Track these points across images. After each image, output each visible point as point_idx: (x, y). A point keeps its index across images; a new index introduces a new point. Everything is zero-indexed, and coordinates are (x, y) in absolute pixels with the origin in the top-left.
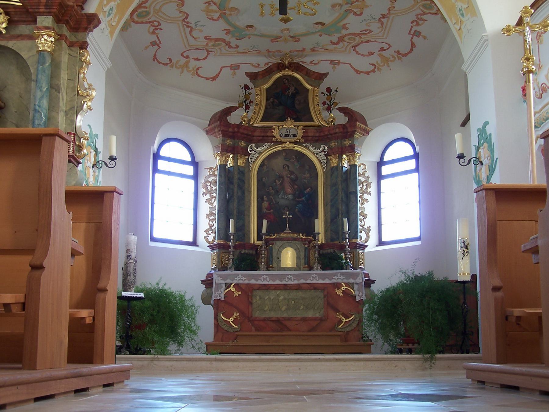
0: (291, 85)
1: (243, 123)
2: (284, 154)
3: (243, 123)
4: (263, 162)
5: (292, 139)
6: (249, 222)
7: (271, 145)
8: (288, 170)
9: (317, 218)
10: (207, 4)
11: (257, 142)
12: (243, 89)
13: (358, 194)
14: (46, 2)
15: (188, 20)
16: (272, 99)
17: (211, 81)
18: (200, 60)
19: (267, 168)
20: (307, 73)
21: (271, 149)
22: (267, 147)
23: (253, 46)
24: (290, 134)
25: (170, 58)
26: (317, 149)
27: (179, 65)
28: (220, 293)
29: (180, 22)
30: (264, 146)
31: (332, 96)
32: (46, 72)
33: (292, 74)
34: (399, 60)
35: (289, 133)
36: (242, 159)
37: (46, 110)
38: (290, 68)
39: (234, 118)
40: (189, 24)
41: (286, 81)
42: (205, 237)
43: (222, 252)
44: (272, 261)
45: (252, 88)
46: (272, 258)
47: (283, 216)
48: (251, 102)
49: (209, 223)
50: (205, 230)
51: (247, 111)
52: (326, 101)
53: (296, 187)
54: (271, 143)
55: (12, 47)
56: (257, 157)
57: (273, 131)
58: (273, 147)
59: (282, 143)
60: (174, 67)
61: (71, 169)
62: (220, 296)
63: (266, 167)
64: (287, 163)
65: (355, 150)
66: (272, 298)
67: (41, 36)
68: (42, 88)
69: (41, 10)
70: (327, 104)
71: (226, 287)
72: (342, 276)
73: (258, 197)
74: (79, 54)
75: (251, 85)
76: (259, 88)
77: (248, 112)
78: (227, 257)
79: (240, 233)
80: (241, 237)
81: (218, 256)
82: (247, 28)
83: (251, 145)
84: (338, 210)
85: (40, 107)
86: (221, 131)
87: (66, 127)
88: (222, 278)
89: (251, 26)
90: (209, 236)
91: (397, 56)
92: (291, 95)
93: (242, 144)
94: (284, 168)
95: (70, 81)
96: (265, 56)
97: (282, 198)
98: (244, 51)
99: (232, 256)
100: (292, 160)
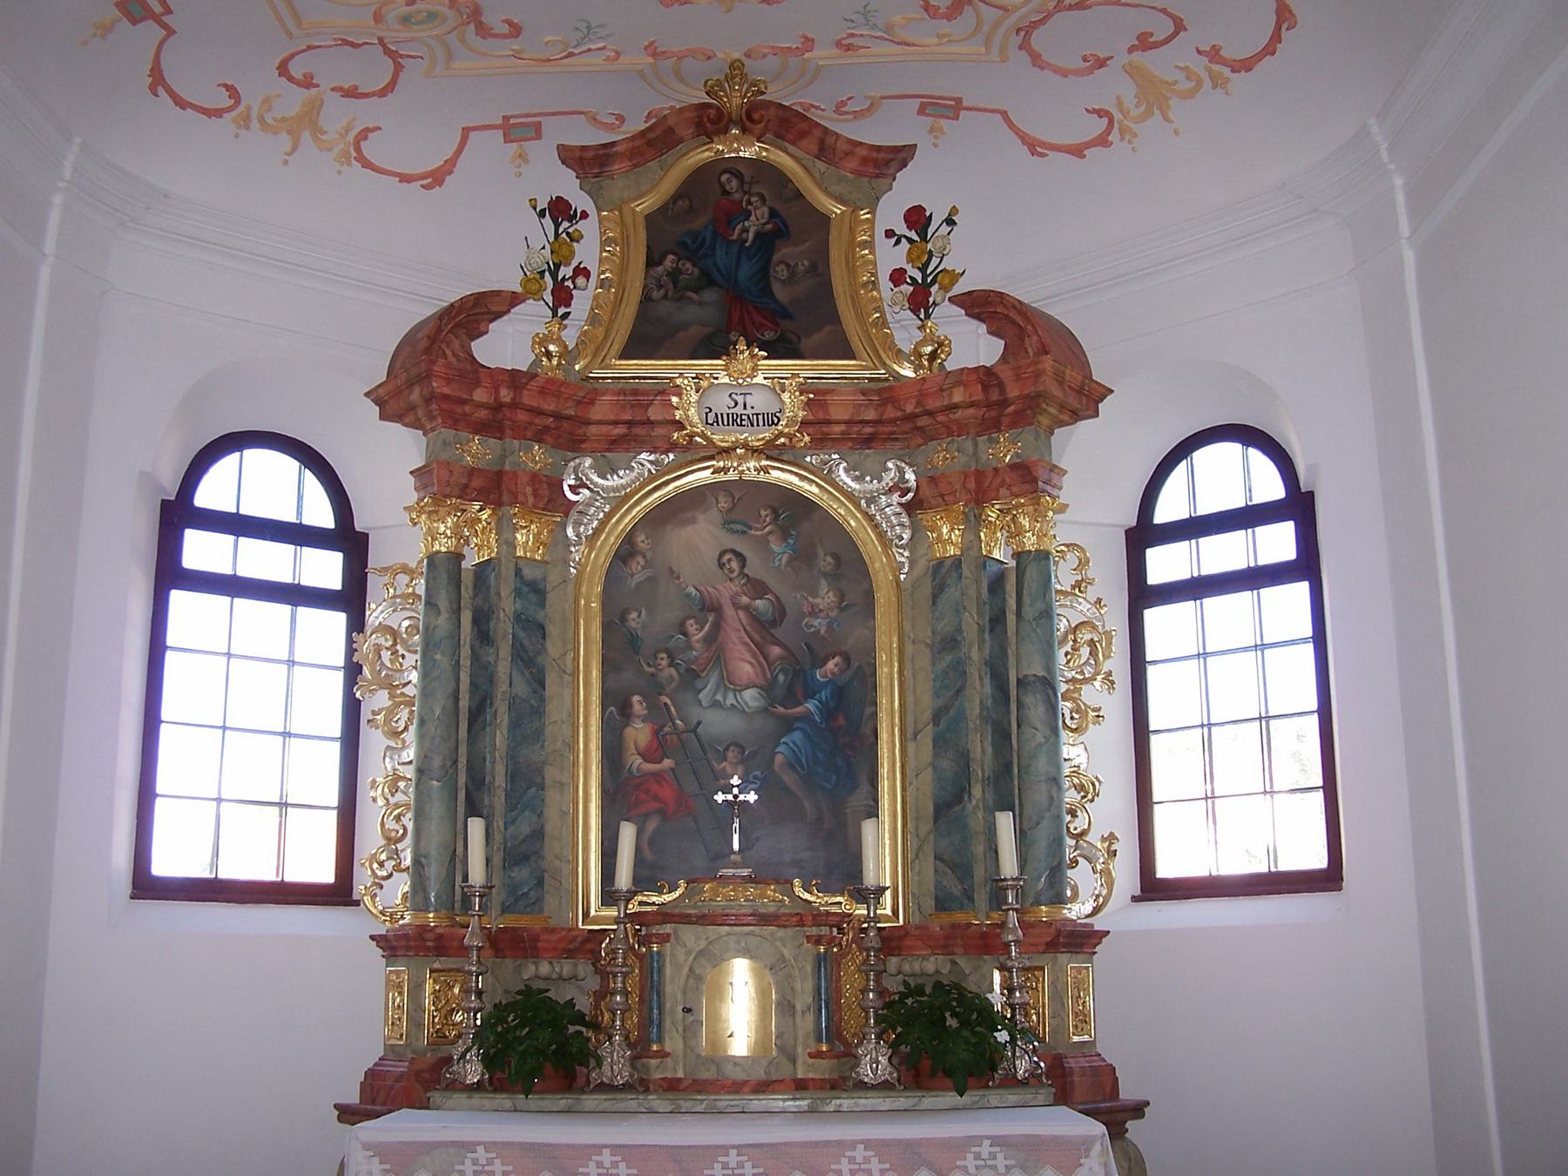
0: (753, 199)
2: (724, 503)
4: (629, 538)
8: (742, 574)
9: (873, 812)
11: (608, 450)
12: (544, 216)
16: (671, 257)
17: (422, 186)
19: (644, 568)
20: (827, 148)
23: (583, 26)
24: (749, 411)
26: (868, 478)
31: (929, 246)
34: (1214, 87)
35: (745, 408)
38: (748, 124)
41: (734, 183)
43: (431, 972)
45: (584, 215)
46: (660, 1009)
47: (716, 797)
48: (581, 271)
51: (561, 311)
52: (905, 266)
53: (776, 651)
60: (255, 124)
65: (1040, 483)
70: (911, 277)
72: (1000, 1156)
75: (580, 200)
77: (566, 315)
78: (876, 316)
79: (522, 873)
80: (525, 890)
84: (964, 759)
88: (388, 1167)
91: (1209, 71)
92: (754, 241)
93: (537, 456)
94: (721, 566)
97: (715, 704)
100: (757, 530)
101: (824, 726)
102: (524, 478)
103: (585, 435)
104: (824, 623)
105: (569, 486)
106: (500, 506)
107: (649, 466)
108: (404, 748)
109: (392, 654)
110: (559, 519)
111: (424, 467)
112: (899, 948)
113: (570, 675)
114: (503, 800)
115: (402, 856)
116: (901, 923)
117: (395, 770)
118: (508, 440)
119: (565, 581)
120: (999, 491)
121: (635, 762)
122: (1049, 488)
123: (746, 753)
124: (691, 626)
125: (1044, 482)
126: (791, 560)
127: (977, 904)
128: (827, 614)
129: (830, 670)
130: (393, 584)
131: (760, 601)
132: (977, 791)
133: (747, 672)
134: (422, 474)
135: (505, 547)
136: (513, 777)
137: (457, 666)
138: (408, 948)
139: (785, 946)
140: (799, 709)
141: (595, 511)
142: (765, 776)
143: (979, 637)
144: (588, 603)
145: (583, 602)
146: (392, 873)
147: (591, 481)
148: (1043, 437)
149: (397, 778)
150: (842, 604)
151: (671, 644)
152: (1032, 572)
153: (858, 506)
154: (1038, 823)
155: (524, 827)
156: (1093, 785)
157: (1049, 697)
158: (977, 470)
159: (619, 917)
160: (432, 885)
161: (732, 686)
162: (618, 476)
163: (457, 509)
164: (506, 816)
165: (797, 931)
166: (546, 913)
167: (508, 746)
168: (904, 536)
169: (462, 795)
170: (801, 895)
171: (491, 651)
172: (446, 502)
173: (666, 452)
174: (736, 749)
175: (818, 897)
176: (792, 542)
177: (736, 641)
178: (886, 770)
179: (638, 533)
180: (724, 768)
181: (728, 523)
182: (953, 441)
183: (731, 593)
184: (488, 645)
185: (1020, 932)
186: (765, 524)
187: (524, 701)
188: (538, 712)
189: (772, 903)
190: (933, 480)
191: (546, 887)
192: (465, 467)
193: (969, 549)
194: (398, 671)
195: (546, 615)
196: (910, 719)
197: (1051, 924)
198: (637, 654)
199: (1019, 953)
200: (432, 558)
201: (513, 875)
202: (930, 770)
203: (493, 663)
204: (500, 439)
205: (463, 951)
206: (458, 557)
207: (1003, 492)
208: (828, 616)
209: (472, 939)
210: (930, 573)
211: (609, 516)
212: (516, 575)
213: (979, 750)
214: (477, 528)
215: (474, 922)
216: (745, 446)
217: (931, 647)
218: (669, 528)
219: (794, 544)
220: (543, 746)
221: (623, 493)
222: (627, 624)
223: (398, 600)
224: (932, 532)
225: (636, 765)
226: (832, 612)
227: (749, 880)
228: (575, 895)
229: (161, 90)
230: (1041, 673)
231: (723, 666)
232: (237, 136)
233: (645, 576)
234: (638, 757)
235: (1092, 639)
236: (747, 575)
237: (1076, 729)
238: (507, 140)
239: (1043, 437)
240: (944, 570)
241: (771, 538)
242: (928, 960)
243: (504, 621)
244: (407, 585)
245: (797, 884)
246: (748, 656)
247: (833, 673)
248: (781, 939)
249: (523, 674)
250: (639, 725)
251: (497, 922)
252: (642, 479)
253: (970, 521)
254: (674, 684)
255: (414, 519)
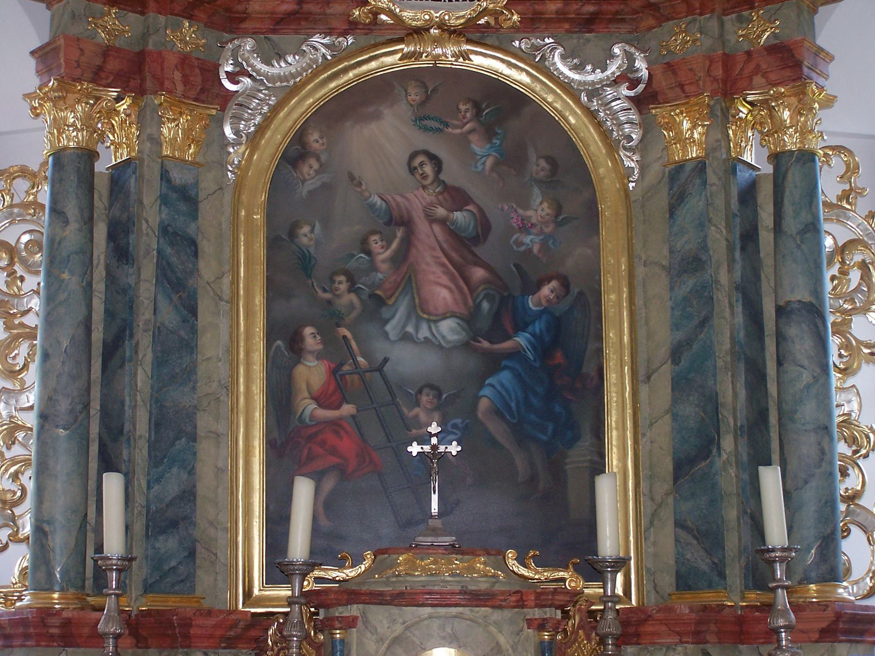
2: (415, 94)
4: (300, 137)
8: (437, 180)
11: (274, 31)
13: (827, 318)
19: (317, 172)
25: (868, 456)
26: (589, 68)
47: (409, 449)
53: (479, 273)
63: (316, 166)
65: (805, 70)
79: (169, 544)
80: (173, 563)
94: (412, 170)
97: (406, 337)
100: (457, 127)
101: (537, 364)
102: (172, 60)
103: (244, 13)
104: (537, 240)
105: (226, 72)
106: (142, 95)
107: (323, 50)
108: (23, 390)
109: (8, 276)
110: (214, 112)
111: (48, 44)
112: (638, 635)
113: (228, 302)
114: (145, 452)
115: (20, 522)
116: (634, 602)
117: (12, 417)
118: (151, 14)
119: (221, 188)
120: (752, 80)
121: (307, 407)
122: (814, 75)
123: (444, 396)
124: (375, 243)
125: (809, 68)
126: (497, 164)
127: (729, 581)
128: (541, 229)
129: (545, 297)
130: (9, 190)
131: (459, 213)
132: (728, 443)
133: (444, 299)
134: (47, 53)
135: (148, 145)
136: (157, 424)
137: (88, 289)
138: (27, 636)
139: (501, 632)
140: (507, 345)
141: (258, 104)
142: (466, 425)
143: (728, 255)
144: (249, 214)
145: (243, 213)
146: (7, 543)
147: (252, 66)
148: (806, 13)
149: (14, 428)
150: (559, 217)
151: (352, 264)
152: (794, 177)
153: (577, 100)
154: (806, 483)
155: (172, 487)
156: (868, 437)
157: (817, 327)
158: (725, 54)
159: (293, 596)
160: (58, 557)
161: (425, 316)
162: (286, 62)
163: (89, 96)
164: (149, 474)
165: (516, 613)
166: (199, 591)
167: (152, 388)
168: (634, 136)
169: (94, 449)
170: (515, 569)
171: (131, 271)
172: (75, 86)
173: (344, 34)
174: (432, 393)
175: (537, 573)
176: (498, 142)
177: (429, 259)
178: (614, 419)
179: (310, 131)
180: (417, 416)
181: (420, 120)
182: (695, 20)
183: (424, 204)
184: (127, 264)
185: (792, 616)
186: (465, 121)
187: (171, 332)
188: (190, 346)
189: (481, 579)
190: (670, 67)
191: (198, 562)
192: (98, 45)
193: (714, 150)
194: (16, 296)
195: (198, 228)
196: (642, 357)
197: (827, 606)
198: (309, 276)
199: (791, 641)
200: (59, 156)
201: (157, 545)
202: (668, 418)
203: (133, 285)
204: (142, 13)
205: (96, 639)
206: (89, 155)
207: (758, 80)
208: (541, 232)
209: (108, 625)
210: (666, 180)
211: (275, 110)
212: (161, 179)
213: (730, 392)
214: (114, 122)
215: (110, 603)
216: (442, 26)
217: (668, 270)
218: (348, 124)
219: (500, 145)
220: (194, 389)
221: (292, 83)
222: (296, 240)
223: (16, 210)
224: (669, 129)
225: (307, 412)
226: (547, 227)
227: (453, 549)
228: (233, 570)
230: (806, 297)
231: (415, 291)
233: (319, 183)
234: (309, 401)
235: (864, 261)
236: (443, 182)
237: (845, 369)
239: (806, 13)
240: (683, 177)
241: (473, 138)
242: (674, 650)
243: (147, 234)
244: (27, 192)
245: (510, 555)
246: (445, 280)
247: (548, 301)
248: (496, 623)
249: (171, 300)
251: (138, 604)
252: (315, 66)
253: (717, 116)
254: (354, 314)
255: (36, 108)
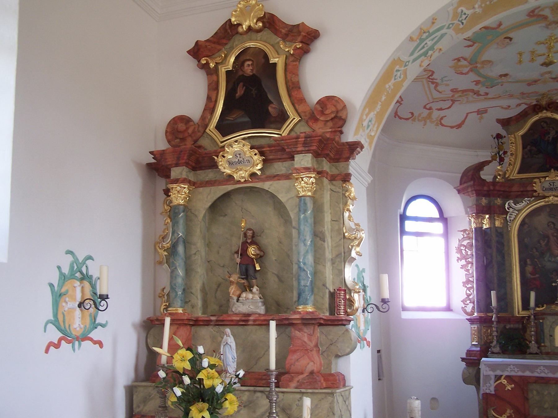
1: (498, 178)
2: (548, 210)
3: (498, 177)
5: (556, 192)
6: (511, 289)
7: (532, 200)
8: (554, 228)
10: (456, 61)
11: (516, 198)
14: (304, 140)
15: (434, 76)
17: (456, 128)
18: (444, 109)
21: (532, 205)
22: (528, 203)
24: (555, 187)
27: (421, 118)
28: (489, 386)
29: (424, 80)
30: (523, 202)
32: (309, 220)
33: (551, 115)
35: (553, 186)
36: (500, 219)
37: (311, 266)
38: (548, 109)
39: (487, 175)
40: (435, 81)
41: (545, 125)
42: (462, 308)
44: (544, 339)
49: (466, 291)
50: (462, 300)
51: (501, 163)
54: (531, 198)
55: (269, 188)
56: (516, 215)
57: (534, 185)
58: (534, 203)
59: (544, 197)
60: (417, 120)
61: (343, 333)
62: (489, 390)
64: (553, 220)
66: (553, 393)
67: (301, 179)
68: (306, 241)
69: (299, 149)
71: (496, 379)
73: (520, 261)
74: (342, 189)
75: (503, 133)
76: (513, 136)
81: (479, 331)
82: (501, 77)
83: (509, 202)
85: (304, 264)
86: (475, 190)
87: (333, 278)
89: (506, 75)
90: (466, 307)
93: (499, 201)
94: (548, 226)
95: (334, 222)
96: (518, 98)
97: (549, 261)
98: (494, 97)
99: (496, 333)
124: (541, 242)
202: (338, 173)
229: (397, 116)
232: (412, 123)
238: (478, 114)
250: (529, 266)
